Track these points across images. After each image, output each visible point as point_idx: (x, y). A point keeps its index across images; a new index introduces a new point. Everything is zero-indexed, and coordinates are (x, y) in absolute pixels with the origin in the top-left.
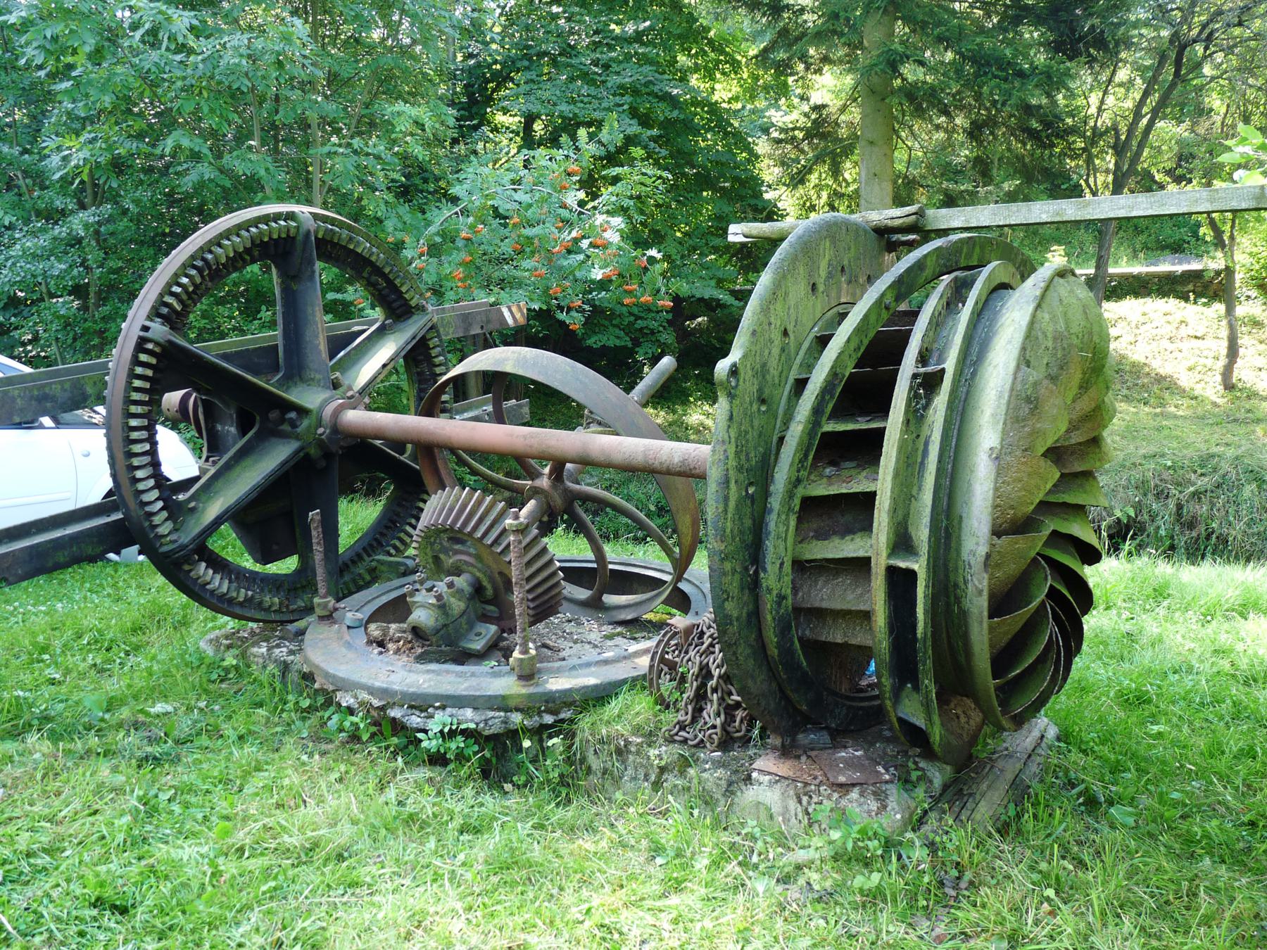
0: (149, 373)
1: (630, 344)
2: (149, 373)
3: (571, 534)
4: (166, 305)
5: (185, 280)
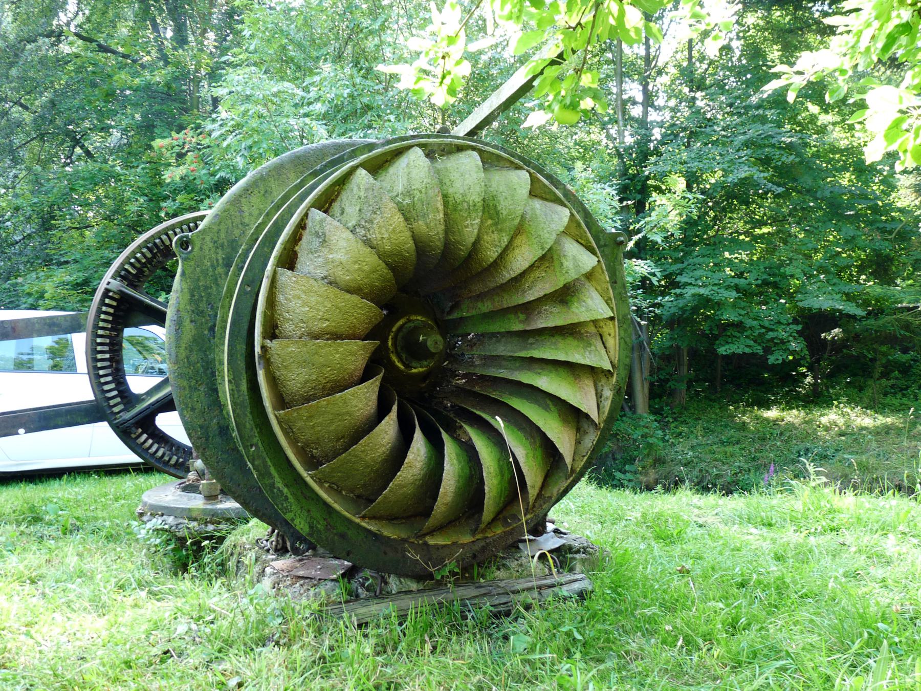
0: (112, 311)
1: (761, 352)
2: (112, 311)
3: (693, 490)
4: (126, 270)
5: (139, 255)
